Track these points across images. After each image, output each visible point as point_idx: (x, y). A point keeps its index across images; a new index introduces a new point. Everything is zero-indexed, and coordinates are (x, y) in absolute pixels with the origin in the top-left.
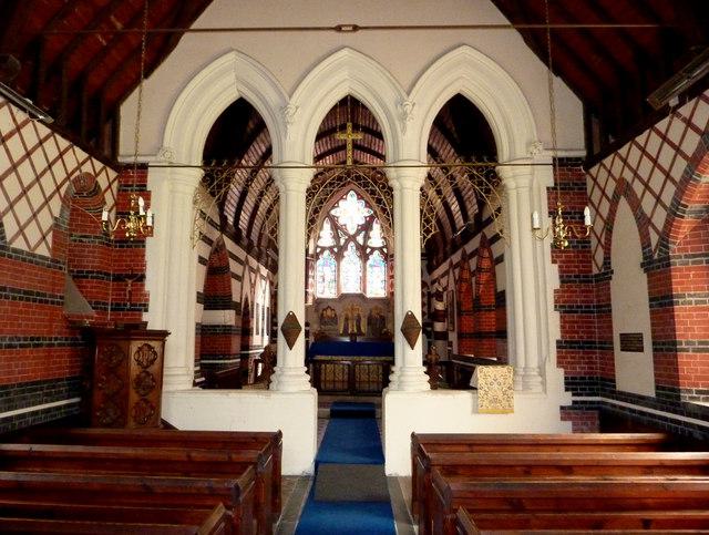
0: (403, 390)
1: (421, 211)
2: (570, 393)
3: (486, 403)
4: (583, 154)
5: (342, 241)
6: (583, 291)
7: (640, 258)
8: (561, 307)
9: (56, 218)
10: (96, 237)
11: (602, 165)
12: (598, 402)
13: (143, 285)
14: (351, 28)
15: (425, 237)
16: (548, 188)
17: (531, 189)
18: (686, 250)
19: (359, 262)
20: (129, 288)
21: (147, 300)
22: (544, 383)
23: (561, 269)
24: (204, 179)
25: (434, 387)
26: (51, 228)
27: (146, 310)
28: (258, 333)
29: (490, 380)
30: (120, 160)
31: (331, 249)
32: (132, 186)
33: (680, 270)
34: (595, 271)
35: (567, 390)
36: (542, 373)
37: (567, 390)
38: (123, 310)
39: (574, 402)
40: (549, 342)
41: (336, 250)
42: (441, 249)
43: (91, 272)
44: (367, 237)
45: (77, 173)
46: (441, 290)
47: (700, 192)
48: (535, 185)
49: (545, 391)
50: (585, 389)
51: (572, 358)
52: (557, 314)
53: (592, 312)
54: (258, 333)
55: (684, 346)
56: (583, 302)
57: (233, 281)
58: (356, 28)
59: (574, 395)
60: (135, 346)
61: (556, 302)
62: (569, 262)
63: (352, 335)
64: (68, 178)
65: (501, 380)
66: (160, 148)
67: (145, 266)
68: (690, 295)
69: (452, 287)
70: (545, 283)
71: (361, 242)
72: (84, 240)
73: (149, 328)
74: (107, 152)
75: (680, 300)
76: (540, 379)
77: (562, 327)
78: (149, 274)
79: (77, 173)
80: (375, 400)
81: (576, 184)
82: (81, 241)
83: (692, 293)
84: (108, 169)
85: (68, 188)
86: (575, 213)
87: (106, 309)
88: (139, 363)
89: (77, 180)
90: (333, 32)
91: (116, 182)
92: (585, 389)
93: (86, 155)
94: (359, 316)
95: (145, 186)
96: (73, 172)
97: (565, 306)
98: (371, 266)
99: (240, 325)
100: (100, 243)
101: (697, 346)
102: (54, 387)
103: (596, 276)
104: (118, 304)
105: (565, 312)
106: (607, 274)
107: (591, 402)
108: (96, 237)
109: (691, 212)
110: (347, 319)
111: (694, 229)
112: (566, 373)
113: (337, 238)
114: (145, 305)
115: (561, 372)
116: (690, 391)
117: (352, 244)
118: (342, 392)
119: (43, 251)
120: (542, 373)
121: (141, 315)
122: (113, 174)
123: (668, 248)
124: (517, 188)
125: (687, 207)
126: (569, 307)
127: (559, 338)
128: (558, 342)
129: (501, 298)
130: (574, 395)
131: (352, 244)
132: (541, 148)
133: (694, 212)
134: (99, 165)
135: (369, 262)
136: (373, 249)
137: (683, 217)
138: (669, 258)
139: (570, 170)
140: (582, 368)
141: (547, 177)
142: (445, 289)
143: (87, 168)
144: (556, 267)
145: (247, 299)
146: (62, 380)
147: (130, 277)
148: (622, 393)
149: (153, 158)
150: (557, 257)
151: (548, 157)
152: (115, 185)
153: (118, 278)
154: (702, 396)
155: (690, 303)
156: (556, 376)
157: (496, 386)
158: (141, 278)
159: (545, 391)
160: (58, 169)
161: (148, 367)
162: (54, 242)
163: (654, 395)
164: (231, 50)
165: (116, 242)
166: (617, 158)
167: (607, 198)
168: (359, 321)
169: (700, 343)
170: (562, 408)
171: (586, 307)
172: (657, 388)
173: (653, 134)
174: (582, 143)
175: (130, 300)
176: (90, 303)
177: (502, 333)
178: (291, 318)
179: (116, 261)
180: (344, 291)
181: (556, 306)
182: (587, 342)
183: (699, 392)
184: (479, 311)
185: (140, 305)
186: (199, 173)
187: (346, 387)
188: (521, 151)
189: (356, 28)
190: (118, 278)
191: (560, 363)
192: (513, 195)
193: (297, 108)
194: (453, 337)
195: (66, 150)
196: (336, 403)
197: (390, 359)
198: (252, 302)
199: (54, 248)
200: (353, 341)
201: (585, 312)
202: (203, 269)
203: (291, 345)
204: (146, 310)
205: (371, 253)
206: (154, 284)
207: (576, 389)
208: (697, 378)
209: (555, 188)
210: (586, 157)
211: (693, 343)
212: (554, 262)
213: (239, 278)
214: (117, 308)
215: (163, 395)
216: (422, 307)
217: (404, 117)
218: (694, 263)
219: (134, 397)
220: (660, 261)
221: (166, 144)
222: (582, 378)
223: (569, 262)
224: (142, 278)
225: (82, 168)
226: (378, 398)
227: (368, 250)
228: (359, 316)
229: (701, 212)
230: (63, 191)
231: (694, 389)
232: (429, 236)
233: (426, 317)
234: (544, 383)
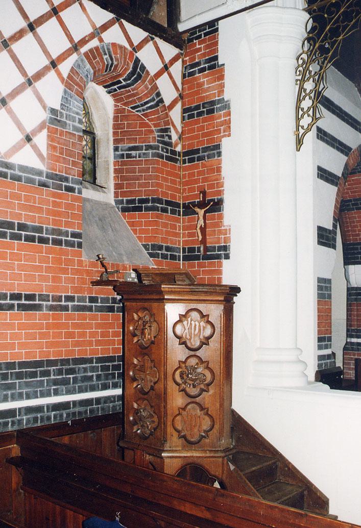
9: (53, 111)
10: (149, 147)
13: (221, 217)
21: (227, 240)
24: (313, 36)
26: (42, 127)
27: (227, 257)
38: (197, 258)
43: (147, 201)
45: (94, 43)
64: (75, 48)
72: (133, 153)
74: (159, 14)
79: (94, 43)
82: (129, 156)
84: (157, 39)
85: (77, 65)
89: (92, 55)
91: (179, 64)
93: (108, 16)
95: (216, 58)
96: (84, 42)
100: (154, 155)
102: (70, 371)
104: (192, 250)
108: (149, 147)
114: (225, 248)
122: (170, 51)
134: (137, 34)
143: (114, 35)
146: (90, 361)
147: (201, 205)
152: (177, 69)
162: (51, 147)
165: (185, 154)
175: (204, 241)
179: (186, 184)
185: (220, 248)
197: (39, 396)
199: (51, 157)
202: (331, 191)
204: (227, 257)
224: (216, 206)
225: (104, 35)
230: (65, 68)
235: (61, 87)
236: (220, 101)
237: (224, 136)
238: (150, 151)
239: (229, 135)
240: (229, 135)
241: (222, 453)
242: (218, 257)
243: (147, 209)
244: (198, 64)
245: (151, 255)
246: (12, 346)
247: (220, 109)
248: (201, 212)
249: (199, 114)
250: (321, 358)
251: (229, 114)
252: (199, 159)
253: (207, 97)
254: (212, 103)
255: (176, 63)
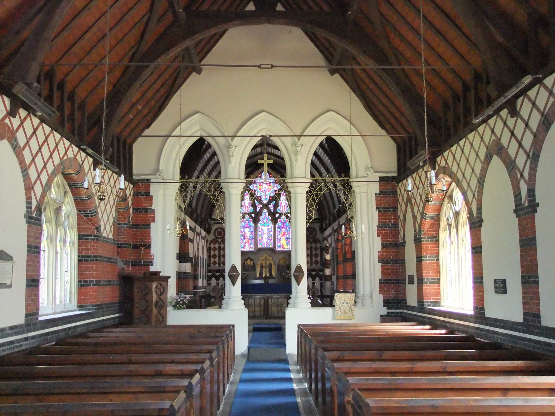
0: (296, 307)
1: (307, 206)
2: (386, 308)
3: (340, 313)
4: (395, 174)
5: (258, 209)
6: (394, 252)
7: (512, 206)
8: (382, 260)
10: (124, 224)
11: (450, 150)
12: (401, 313)
13: (150, 251)
14: (270, 66)
15: (308, 221)
16: (376, 194)
17: (367, 193)
18: (427, 234)
19: (271, 224)
20: (143, 252)
21: (153, 259)
22: (372, 303)
23: (382, 240)
25: (312, 306)
27: (152, 265)
28: (200, 278)
29: (342, 301)
30: (134, 177)
31: (250, 214)
32: (141, 193)
33: (425, 244)
34: (400, 241)
35: (384, 306)
36: (371, 297)
37: (384, 306)
39: (388, 313)
40: (375, 280)
41: (253, 215)
42: (328, 219)
44: (276, 206)
46: (328, 245)
47: (431, 208)
48: (369, 191)
49: (373, 307)
50: (393, 306)
51: (387, 288)
52: (380, 265)
53: (399, 263)
54: (200, 278)
55: (426, 281)
56: (393, 257)
57: (190, 243)
58: (273, 66)
59: (387, 309)
60: (154, 284)
61: (379, 258)
62: (387, 235)
63: (266, 278)
65: (348, 301)
66: (157, 171)
67: (151, 239)
68: (429, 257)
69: (333, 245)
70: (374, 248)
71: (272, 209)
73: (161, 275)
75: (425, 259)
76: (370, 300)
77: (382, 272)
78: (153, 244)
80: (281, 321)
81: (392, 192)
83: (430, 255)
86: (390, 208)
87: (129, 265)
88: (157, 293)
90: (257, 68)
92: (393, 306)
94: (270, 264)
97: (384, 261)
98: (279, 227)
99: (193, 272)
101: (431, 281)
103: (401, 243)
105: (384, 263)
106: (403, 244)
107: (397, 313)
108: (124, 224)
109: (429, 217)
110: (262, 266)
111: (432, 224)
112: (383, 297)
113: (254, 206)
115: (381, 296)
116: (427, 302)
117: (265, 211)
118: (260, 317)
119: (111, 237)
120: (371, 297)
121: (149, 268)
123: (421, 233)
124: (360, 193)
125: (426, 214)
126: (387, 261)
127: (380, 277)
128: (380, 280)
129: (353, 254)
130: (387, 309)
131: (265, 202)
132: (372, 171)
133: (431, 217)
135: (279, 224)
136: (281, 215)
137: (425, 219)
138: (421, 238)
139: (388, 184)
140: (393, 294)
141: (376, 188)
142: (330, 245)
144: (380, 238)
145: (195, 254)
148: (408, 306)
149: (154, 177)
150: (380, 233)
151: (376, 177)
153: (135, 247)
154: (432, 304)
155: (429, 260)
156: (379, 298)
157: (345, 304)
158: (148, 246)
159: (373, 307)
160: (55, 156)
161: (161, 295)
163: (417, 306)
164: (196, 112)
165: (133, 225)
166: (526, 100)
167: (531, 131)
168: (270, 268)
169: (432, 279)
170: (381, 316)
171: (396, 260)
172: (525, 314)
173: (542, 89)
174: (395, 169)
176: (123, 261)
177: (353, 276)
178: (234, 268)
180: (260, 246)
181: (379, 260)
182: (396, 280)
183: (431, 302)
184: (346, 262)
185: (149, 262)
186: (178, 185)
187: (262, 314)
188: (362, 172)
189: (273, 66)
190: (135, 247)
191: (381, 292)
192: (358, 196)
193: (236, 147)
194: (334, 278)
195: (25, 118)
196: (255, 324)
198: (198, 256)
200: (266, 284)
201: (395, 263)
203: (234, 283)
204: (152, 265)
205: (279, 217)
206: (156, 250)
207: (389, 306)
208: (431, 296)
209: (380, 194)
210: (398, 175)
211: (429, 279)
212: (378, 236)
213: (192, 241)
214: (135, 264)
215: (167, 312)
216: (307, 257)
217: (296, 153)
218: (431, 241)
219: (155, 311)
220: (419, 238)
221: (160, 169)
222: (392, 299)
223: (387, 235)
224: (149, 246)
226: (283, 320)
227: (277, 215)
228: (270, 264)
229: (433, 217)
231: (429, 301)
232: (311, 220)
233: (309, 264)
234: (372, 303)
235: (35, 188)
236: (150, 209)
237: (152, 222)
238: (125, 226)
239: (154, 222)
240: (154, 222)
241: (222, 285)
242: (148, 265)
243: (124, 247)
244: (141, 193)
245: (125, 264)
246: (93, 292)
247: (150, 212)
248: (143, 249)
249: (141, 212)
250: (211, 281)
251: (154, 214)
252: (140, 228)
253: (144, 206)
254: (147, 209)
255: (52, 171)
